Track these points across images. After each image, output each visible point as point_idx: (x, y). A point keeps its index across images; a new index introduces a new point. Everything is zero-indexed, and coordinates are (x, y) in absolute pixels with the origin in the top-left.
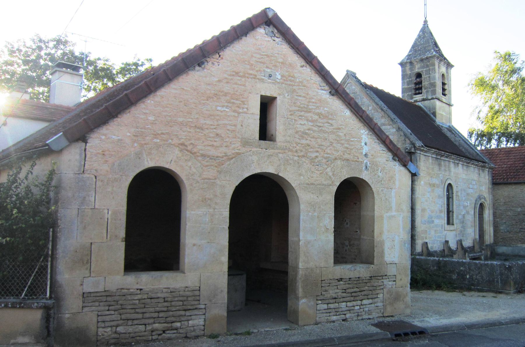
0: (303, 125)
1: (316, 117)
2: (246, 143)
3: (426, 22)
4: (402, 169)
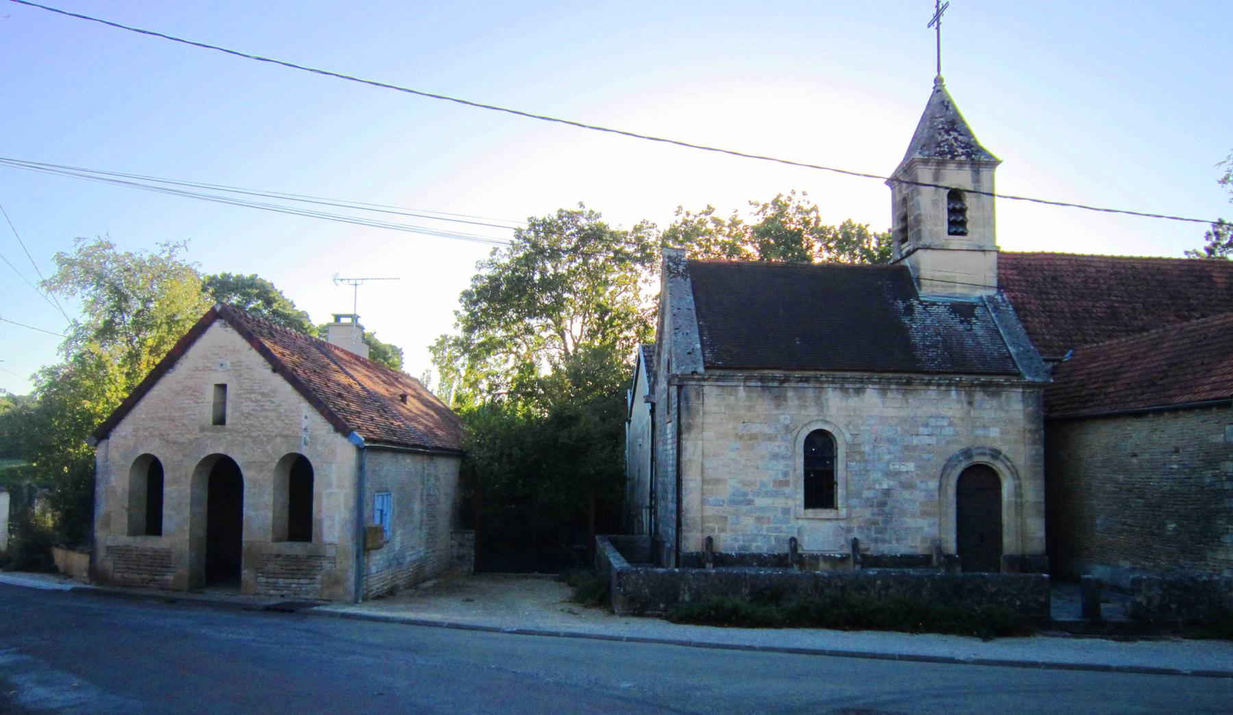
0: (247, 407)
1: (259, 397)
2: (203, 429)
3: (938, 81)
4: (345, 440)
